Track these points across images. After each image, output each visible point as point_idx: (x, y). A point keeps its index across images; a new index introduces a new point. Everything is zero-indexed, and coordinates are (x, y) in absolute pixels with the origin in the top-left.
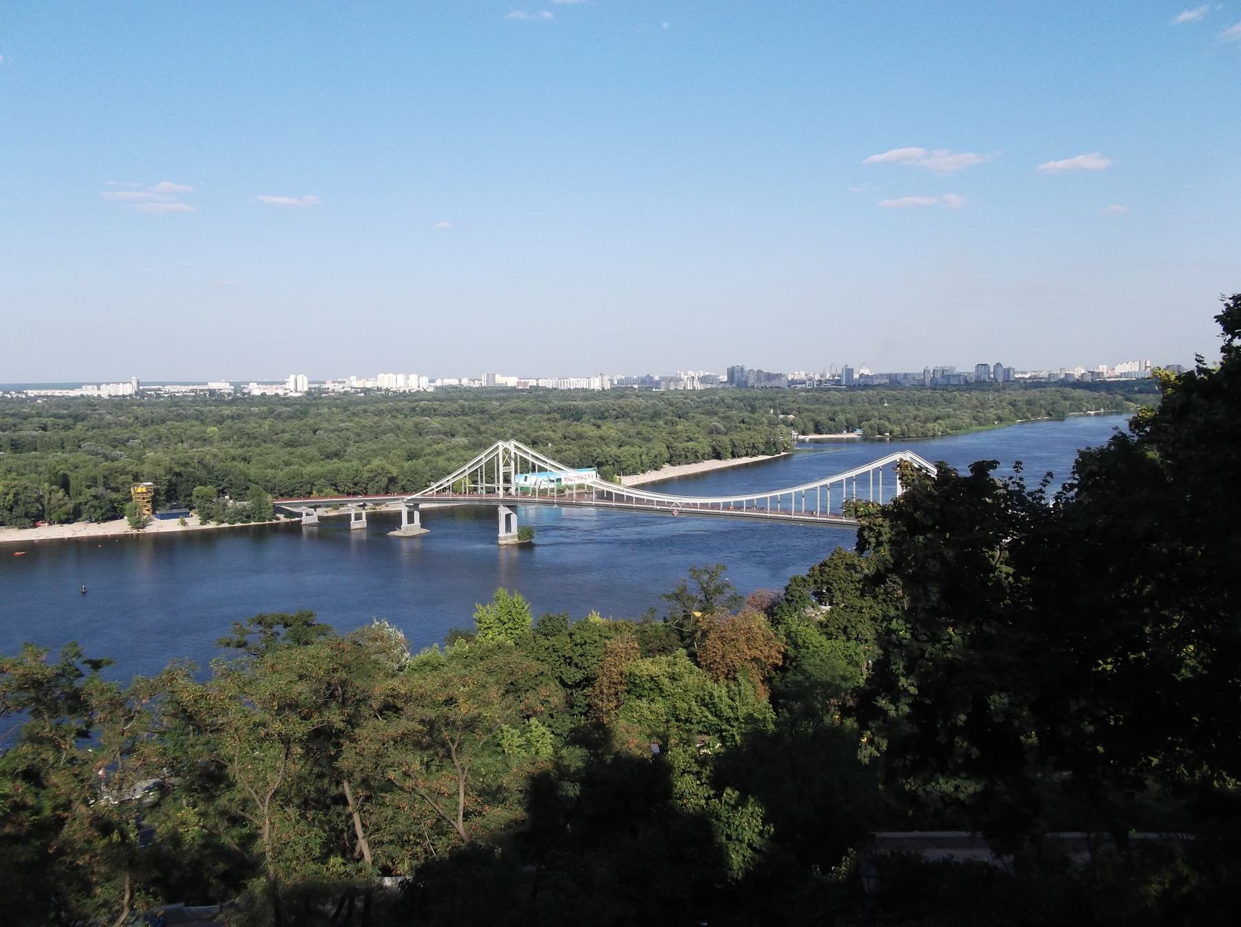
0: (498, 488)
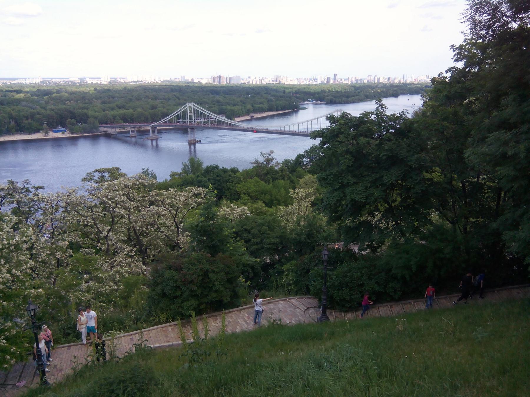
0: (187, 121)
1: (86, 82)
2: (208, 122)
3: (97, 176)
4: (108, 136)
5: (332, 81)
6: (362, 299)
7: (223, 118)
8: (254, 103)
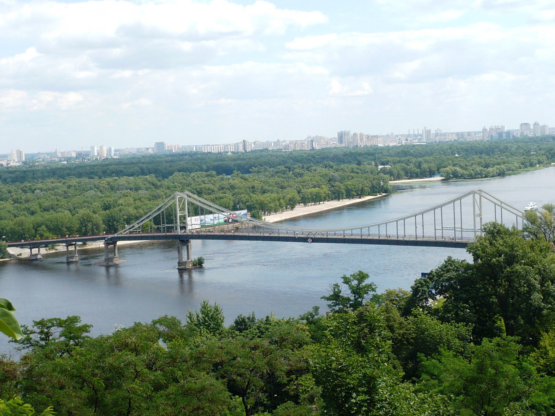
6: (91, 211)
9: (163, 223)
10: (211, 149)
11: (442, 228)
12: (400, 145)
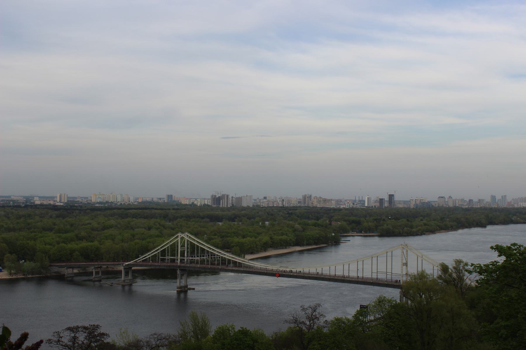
0: (177, 259)
1: (34, 203)
2: (208, 261)
3: (68, 338)
4: (61, 278)
5: (386, 204)
7: (228, 256)
8: (274, 234)
9: (168, 255)
10: (207, 201)
11: (377, 272)
12: (348, 207)
